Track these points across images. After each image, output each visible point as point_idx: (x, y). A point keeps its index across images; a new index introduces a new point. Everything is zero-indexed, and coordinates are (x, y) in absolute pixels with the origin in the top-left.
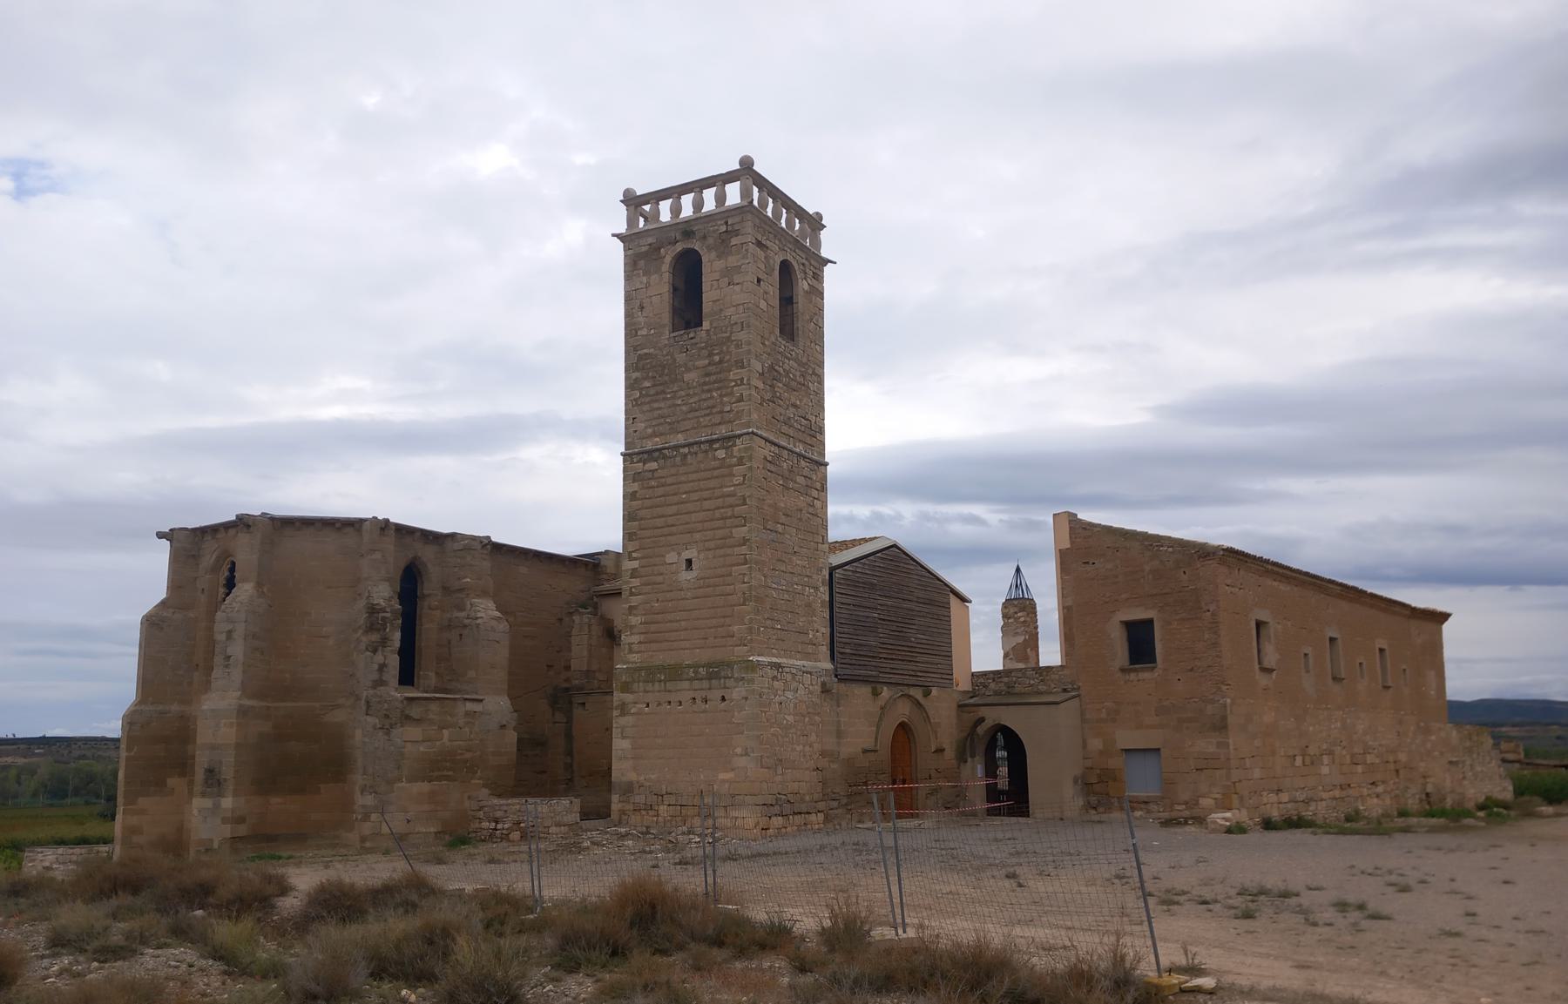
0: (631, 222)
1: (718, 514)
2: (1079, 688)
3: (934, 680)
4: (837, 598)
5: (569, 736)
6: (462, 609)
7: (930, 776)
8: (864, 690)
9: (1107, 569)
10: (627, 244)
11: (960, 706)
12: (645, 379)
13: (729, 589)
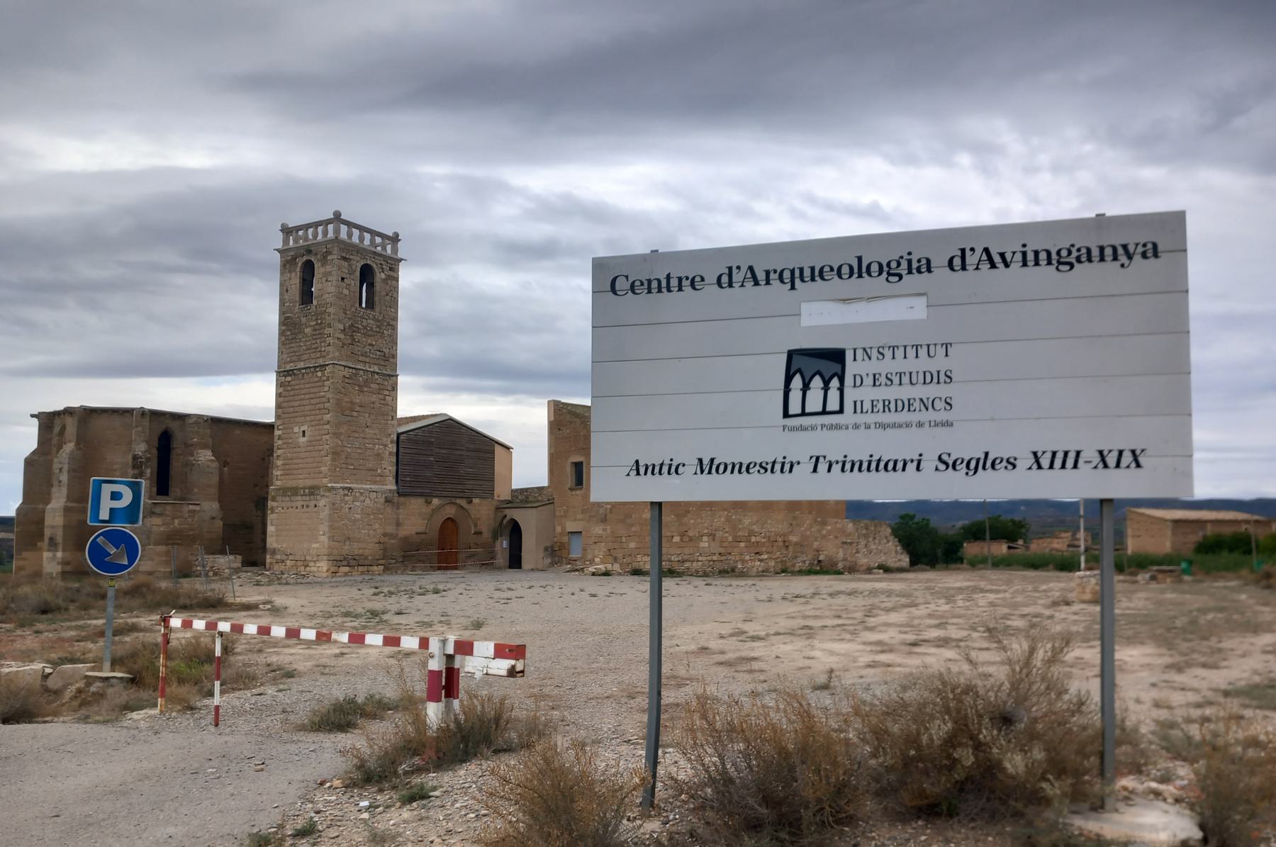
0: (286, 241)
1: (317, 406)
4: (401, 450)
8: (421, 501)
13: (321, 447)
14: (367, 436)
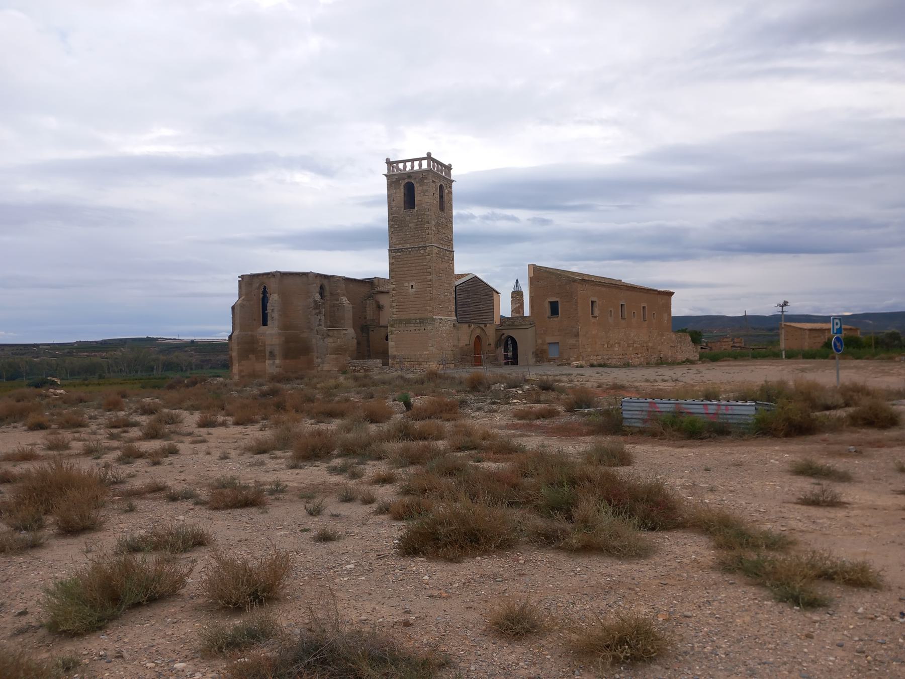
1: (421, 271)
2: (535, 323)
4: (458, 296)
5: (368, 341)
6: (337, 300)
8: (467, 325)
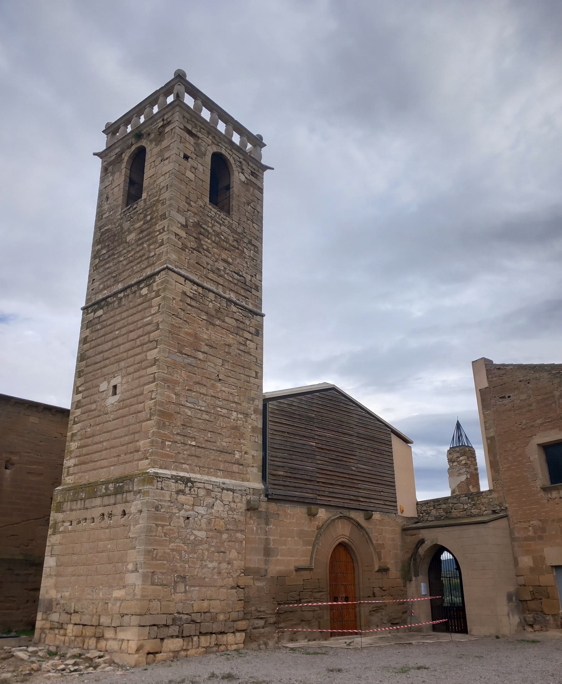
1: (138, 342)
3: (377, 506)
4: (269, 425)
7: (374, 593)
8: (300, 511)
9: (521, 400)
10: (103, 159)
11: (405, 530)
12: (102, 248)
14: (220, 395)
